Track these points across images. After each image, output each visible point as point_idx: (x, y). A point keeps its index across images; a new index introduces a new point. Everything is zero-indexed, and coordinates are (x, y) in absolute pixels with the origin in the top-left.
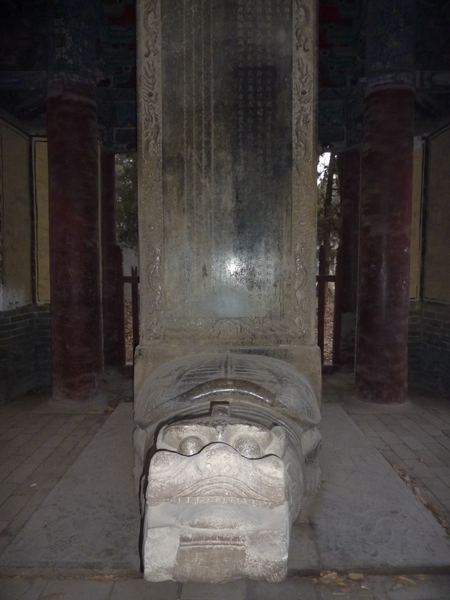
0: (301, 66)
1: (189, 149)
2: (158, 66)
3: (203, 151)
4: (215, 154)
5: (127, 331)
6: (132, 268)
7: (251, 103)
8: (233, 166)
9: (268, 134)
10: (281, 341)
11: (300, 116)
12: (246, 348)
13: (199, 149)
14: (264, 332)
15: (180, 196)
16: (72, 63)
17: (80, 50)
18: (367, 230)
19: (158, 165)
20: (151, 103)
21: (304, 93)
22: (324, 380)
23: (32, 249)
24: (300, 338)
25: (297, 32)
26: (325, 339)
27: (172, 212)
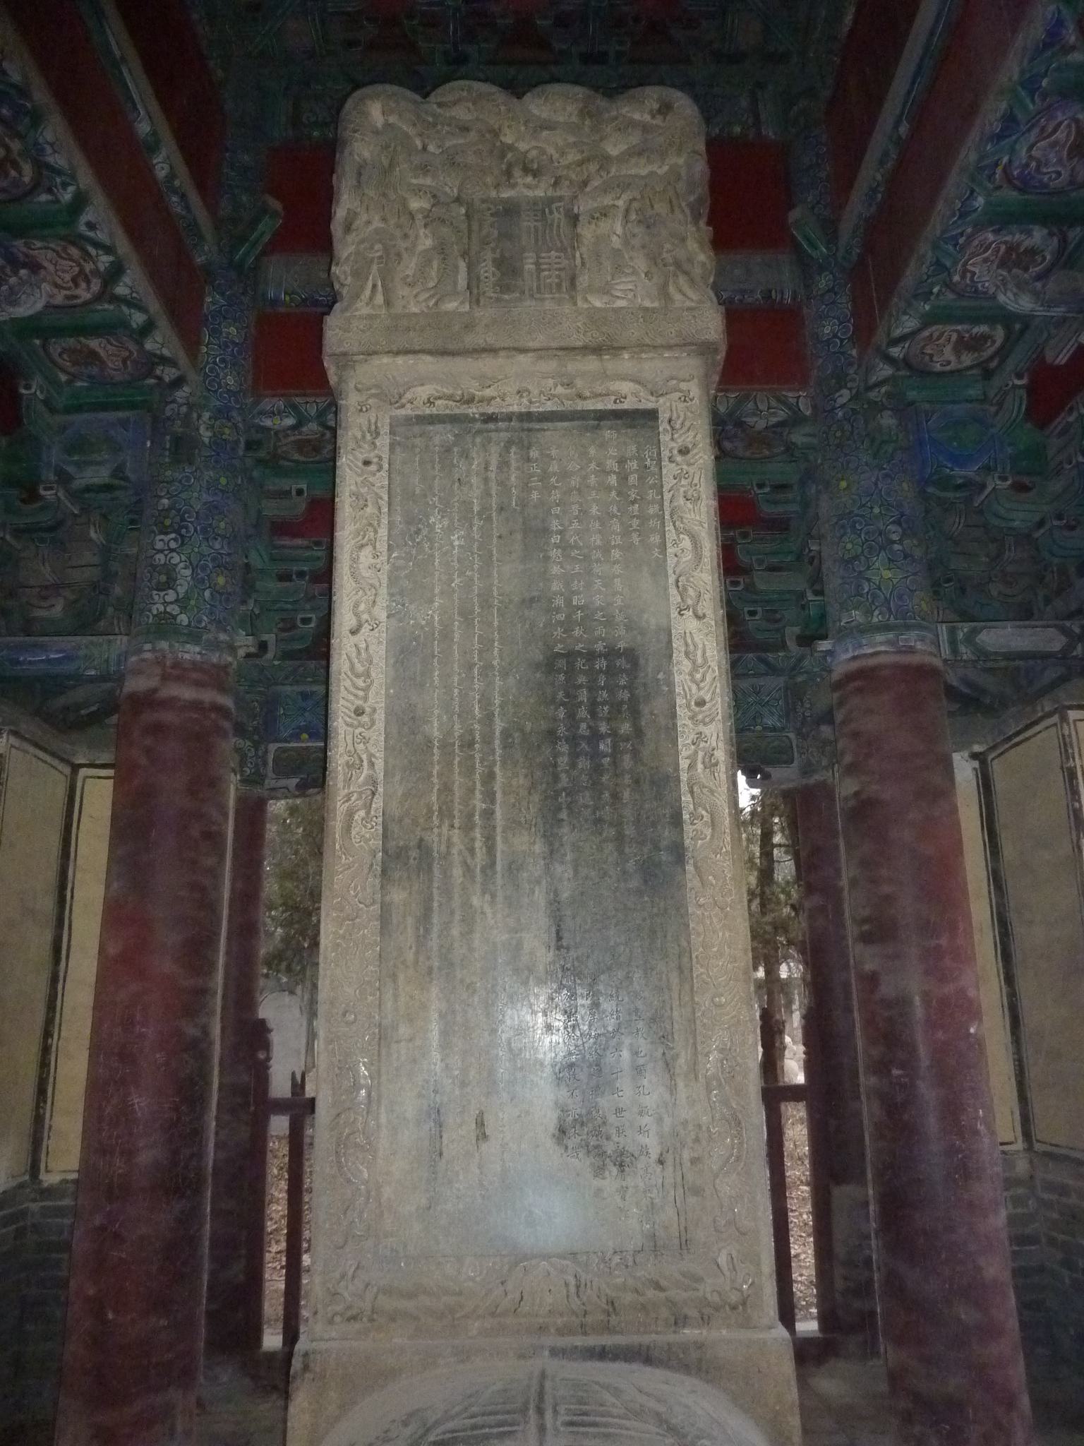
0: (692, 647)
1: (445, 829)
2: (379, 652)
3: (477, 834)
4: (505, 840)
5: (270, 1226)
6: (293, 1074)
7: (583, 726)
8: (547, 866)
9: (626, 794)
10: (686, 1317)
11: (696, 752)
12: (593, 1341)
13: (468, 827)
14: (637, 1291)
15: (422, 940)
16: (186, 622)
17: (207, 594)
18: (872, 980)
19: (372, 865)
20: (360, 730)
21: (701, 703)
22: (802, 1381)
23: (47, 1034)
24: (734, 1308)
25: (677, 581)
26: (792, 1240)
27: (401, 977)
